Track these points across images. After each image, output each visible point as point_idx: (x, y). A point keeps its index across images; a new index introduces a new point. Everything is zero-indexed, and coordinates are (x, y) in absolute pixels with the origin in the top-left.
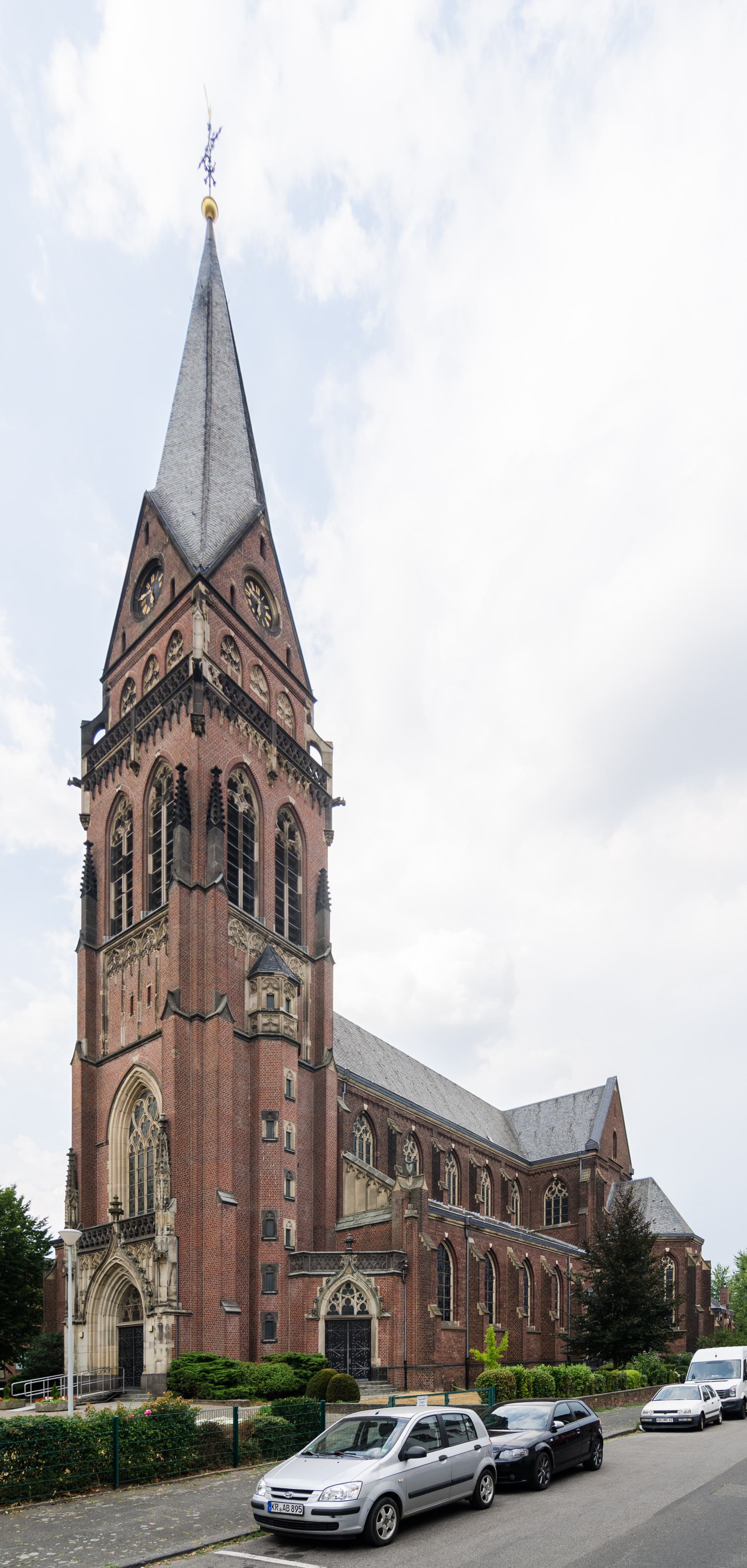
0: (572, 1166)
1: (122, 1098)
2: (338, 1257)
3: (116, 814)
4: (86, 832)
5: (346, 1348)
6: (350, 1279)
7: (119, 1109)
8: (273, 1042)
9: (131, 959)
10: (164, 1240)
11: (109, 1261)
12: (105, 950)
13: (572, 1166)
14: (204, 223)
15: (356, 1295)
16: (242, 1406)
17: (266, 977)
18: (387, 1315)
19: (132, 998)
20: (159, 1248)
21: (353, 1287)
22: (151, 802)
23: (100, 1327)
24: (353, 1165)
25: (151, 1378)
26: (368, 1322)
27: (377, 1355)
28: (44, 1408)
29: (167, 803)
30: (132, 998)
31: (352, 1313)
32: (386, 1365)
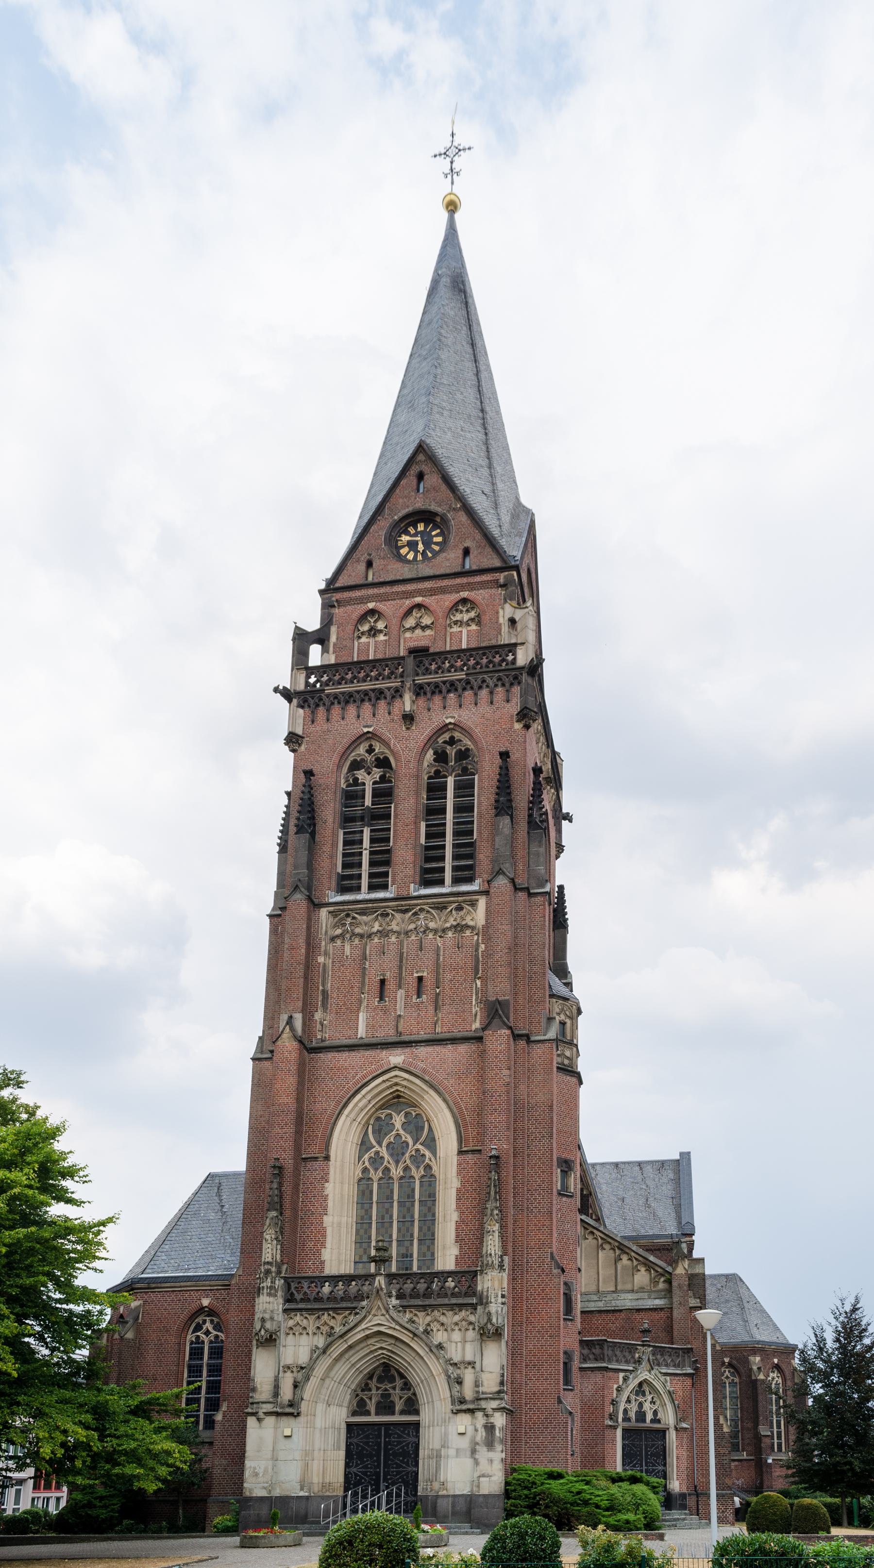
0: (663, 1249)
1: (361, 1105)
2: (632, 1348)
3: (353, 754)
4: (292, 754)
5: (642, 1466)
6: (647, 1377)
7: (353, 1116)
8: (568, 1078)
9: (384, 934)
10: (500, 1309)
11: (363, 1326)
12: (331, 909)
13: (663, 1249)
14: (445, 215)
15: (649, 1398)
16: (849, 1541)
17: (561, 1002)
18: (684, 1425)
19: (383, 982)
20: (494, 1320)
21: (646, 1388)
22: (426, 764)
23: (319, 1422)
24: (595, 1231)
25: (462, 1501)
26: (663, 1432)
27: (675, 1477)
28: (426, 1542)
29: (455, 777)
30: (383, 982)
31: (644, 1421)
32: (685, 1491)
